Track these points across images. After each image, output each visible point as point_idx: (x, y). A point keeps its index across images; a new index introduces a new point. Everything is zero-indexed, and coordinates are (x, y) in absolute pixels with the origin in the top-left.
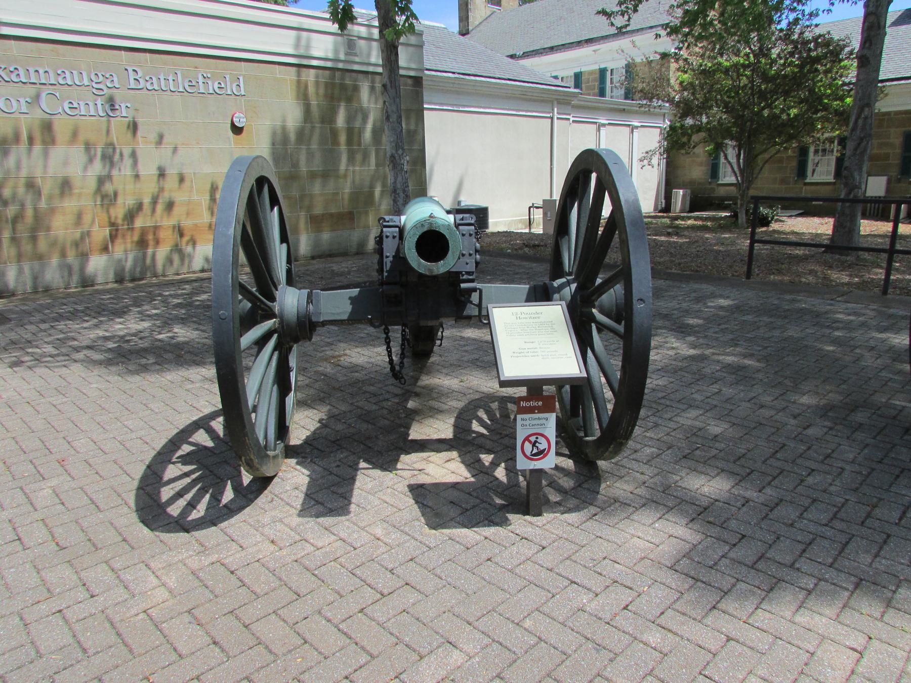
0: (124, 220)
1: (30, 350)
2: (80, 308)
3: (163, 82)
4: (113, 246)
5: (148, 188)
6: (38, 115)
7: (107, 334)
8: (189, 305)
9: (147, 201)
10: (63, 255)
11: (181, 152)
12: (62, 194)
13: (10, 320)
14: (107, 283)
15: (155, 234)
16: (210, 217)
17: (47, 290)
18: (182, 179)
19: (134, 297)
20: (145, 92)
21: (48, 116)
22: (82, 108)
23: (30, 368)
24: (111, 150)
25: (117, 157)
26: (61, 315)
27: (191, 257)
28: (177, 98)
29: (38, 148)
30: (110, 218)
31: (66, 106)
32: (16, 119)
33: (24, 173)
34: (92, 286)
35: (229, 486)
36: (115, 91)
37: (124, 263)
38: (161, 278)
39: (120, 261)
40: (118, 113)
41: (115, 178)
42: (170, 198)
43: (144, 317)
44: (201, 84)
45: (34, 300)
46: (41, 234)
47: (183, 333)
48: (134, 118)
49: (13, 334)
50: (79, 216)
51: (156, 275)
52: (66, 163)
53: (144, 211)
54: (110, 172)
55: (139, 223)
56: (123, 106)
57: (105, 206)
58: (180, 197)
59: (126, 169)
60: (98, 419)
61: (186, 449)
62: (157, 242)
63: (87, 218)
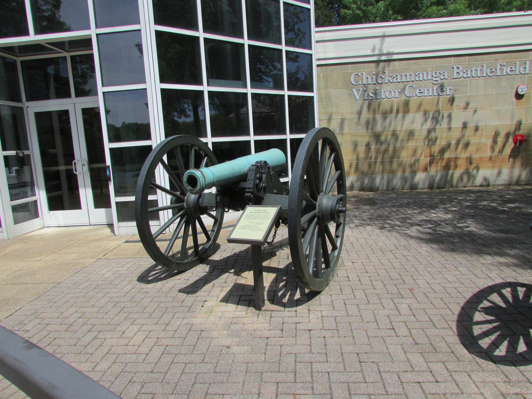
0: (438, 153)
1: (388, 222)
2: (411, 201)
3: (474, 72)
4: (430, 168)
5: (455, 135)
6: (403, 98)
7: (428, 219)
8: (474, 207)
9: (453, 142)
10: (404, 171)
11: (478, 112)
12: (408, 139)
13: (377, 204)
14: (424, 188)
15: (455, 162)
16: (491, 153)
17: (393, 189)
18: (477, 129)
19: (440, 199)
20: (462, 79)
21: (407, 98)
22: (426, 92)
23: (389, 231)
24: (437, 114)
25: (440, 118)
26: (402, 204)
27: (474, 177)
28: (481, 81)
29: (400, 115)
30: (431, 152)
31: (417, 92)
32: (393, 101)
33: (392, 128)
34: (416, 189)
35: (521, 341)
36: (445, 80)
37: (434, 178)
38: (455, 188)
39: (433, 176)
40: (444, 93)
41: (437, 130)
42: (468, 141)
43: (447, 211)
44: (498, 70)
45: (386, 194)
46: (395, 160)
47: (472, 226)
48: (453, 95)
49: (379, 211)
50: (415, 151)
51: (452, 186)
52: (413, 122)
53: (451, 148)
54: (435, 126)
55: (447, 155)
56: (448, 89)
57: (430, 145)
58: (473, 140)
59: (444, 124)
60: (429, 269)
61: (486, 304)
62: (456, 167)
63: (419, 152)
